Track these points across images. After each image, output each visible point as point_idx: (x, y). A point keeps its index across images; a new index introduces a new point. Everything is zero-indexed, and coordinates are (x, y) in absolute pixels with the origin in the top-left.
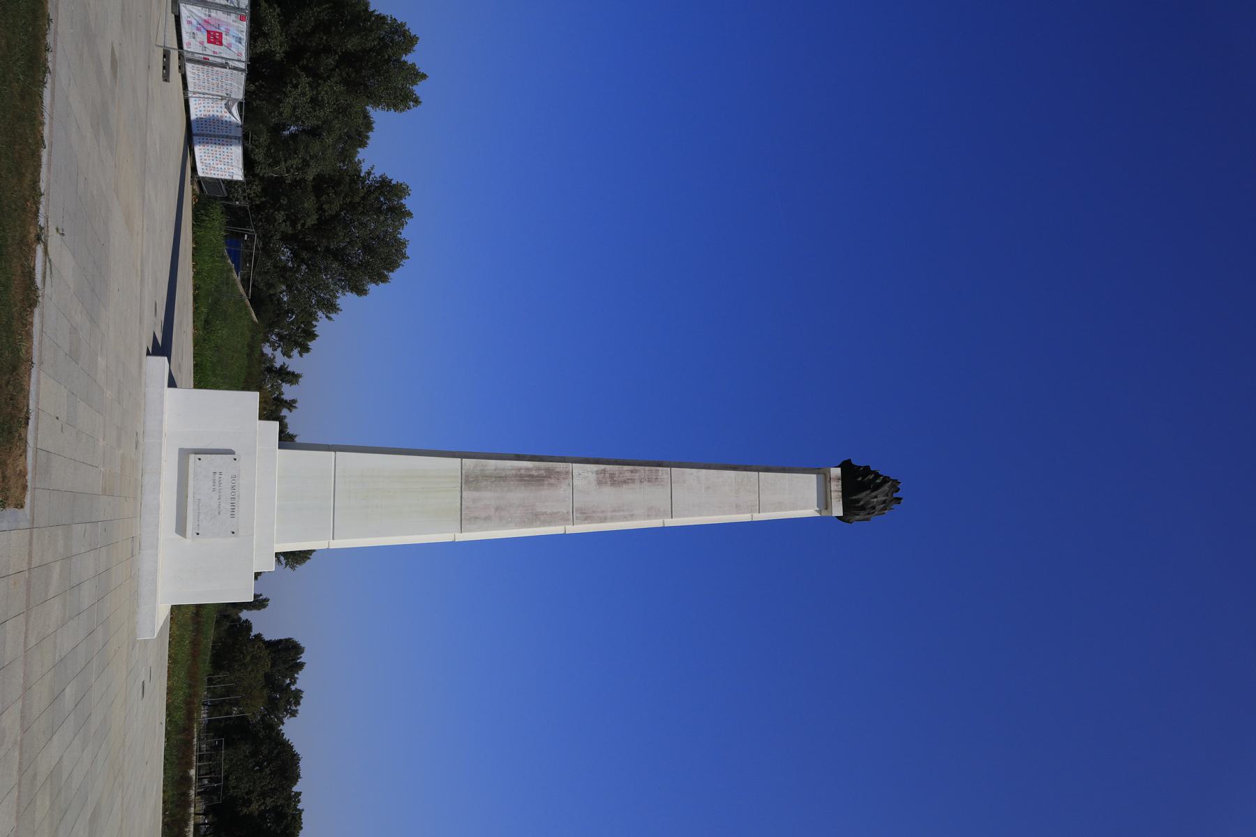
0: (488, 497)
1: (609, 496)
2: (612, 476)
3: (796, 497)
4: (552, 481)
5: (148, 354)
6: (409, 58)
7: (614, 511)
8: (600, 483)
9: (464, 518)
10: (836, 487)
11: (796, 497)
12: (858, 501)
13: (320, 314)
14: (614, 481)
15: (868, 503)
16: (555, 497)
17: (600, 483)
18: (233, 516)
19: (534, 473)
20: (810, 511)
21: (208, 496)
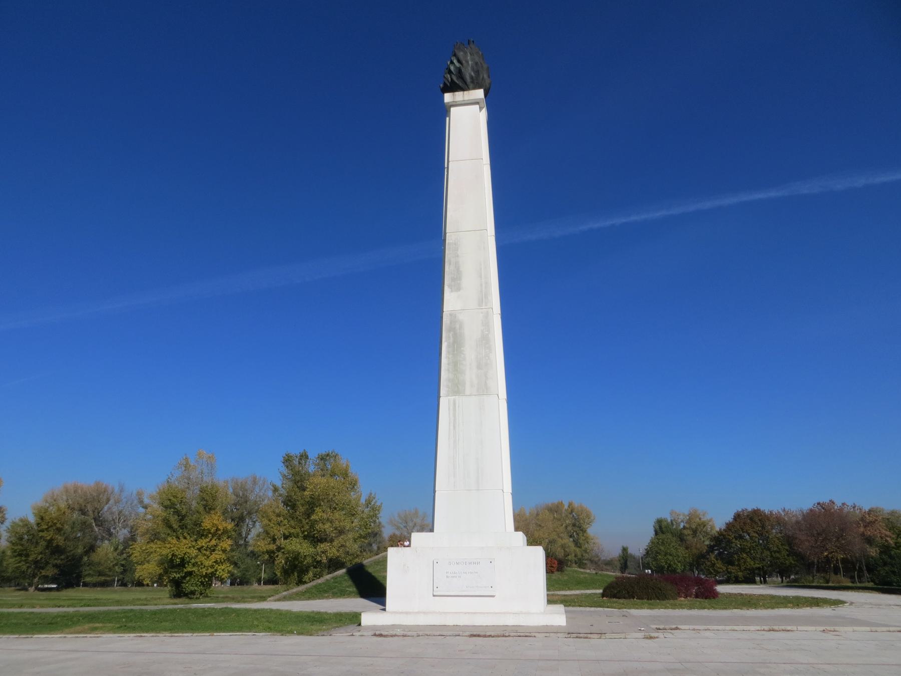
0: (470, 375)
1: (469, 281)
2: (453, 280)
3: (467, 124)
4: (458, 326)
5: (384, 610)
6: (32, 519)
7: (481, 277)
8: (459, 289)
9: (484, 389)
10: (459, 96)
11: (467, 124)
12: (472, 77)
13: (194, 504)
14: (458, 278)
15: (473, 69)
16: (471, 332)
17: (459, 289)
18: (375, 635)
19: (451, 340)
20: (482, 116)
21: (467, 559)
